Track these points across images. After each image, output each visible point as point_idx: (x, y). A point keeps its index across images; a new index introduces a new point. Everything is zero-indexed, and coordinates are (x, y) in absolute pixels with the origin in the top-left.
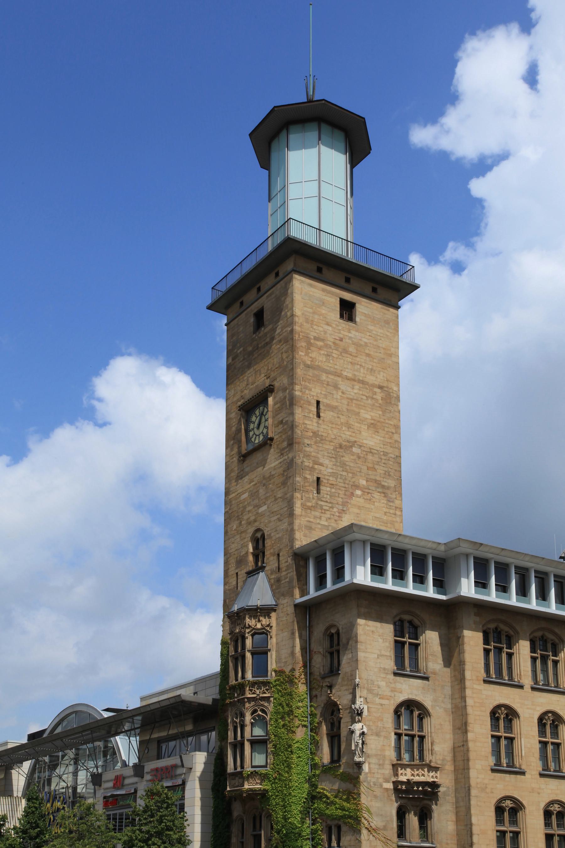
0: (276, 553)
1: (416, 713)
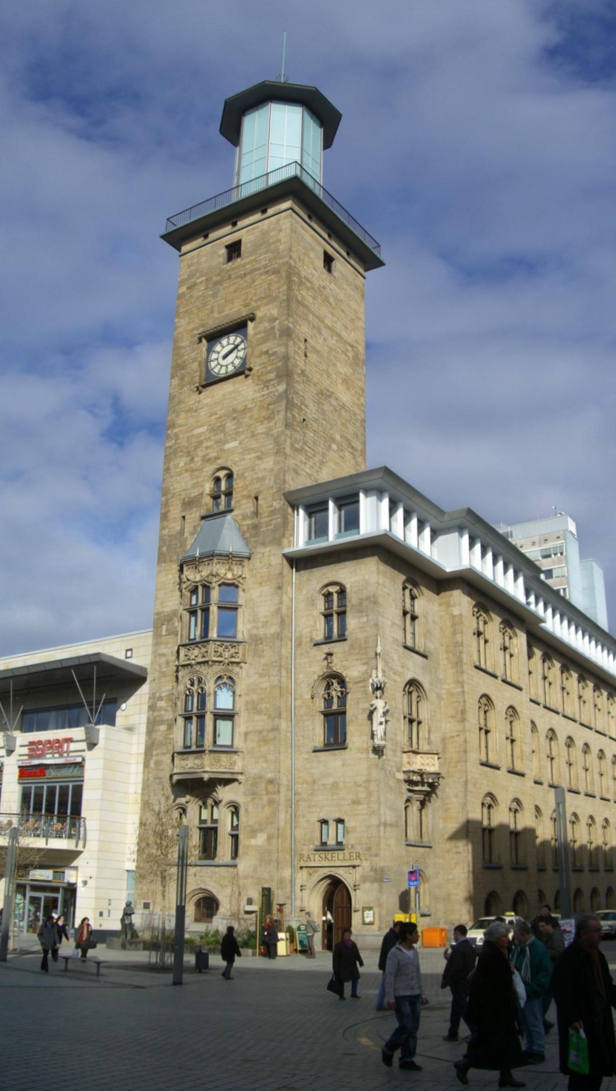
0: (253, 495)
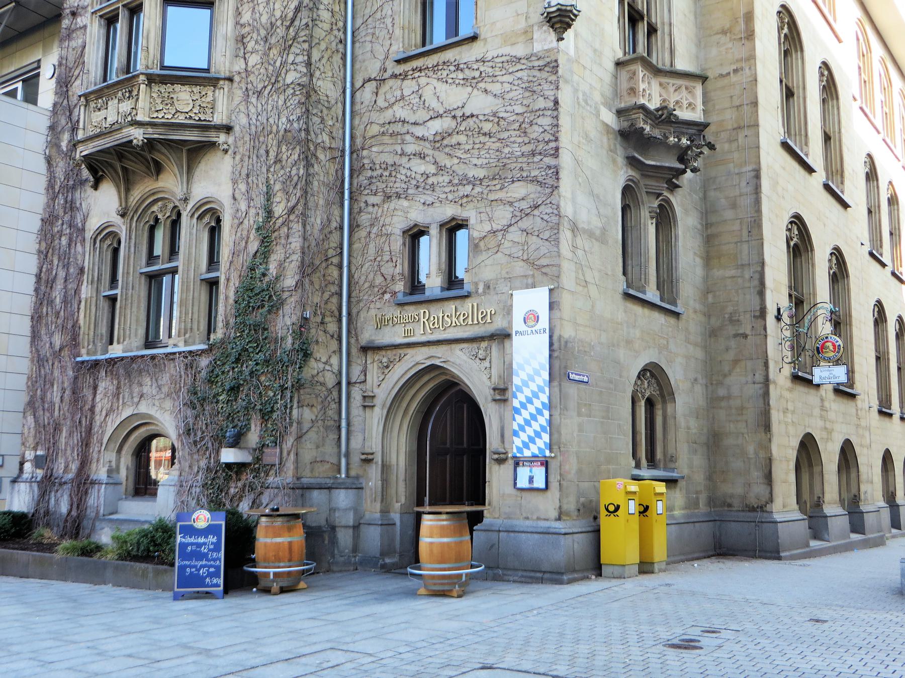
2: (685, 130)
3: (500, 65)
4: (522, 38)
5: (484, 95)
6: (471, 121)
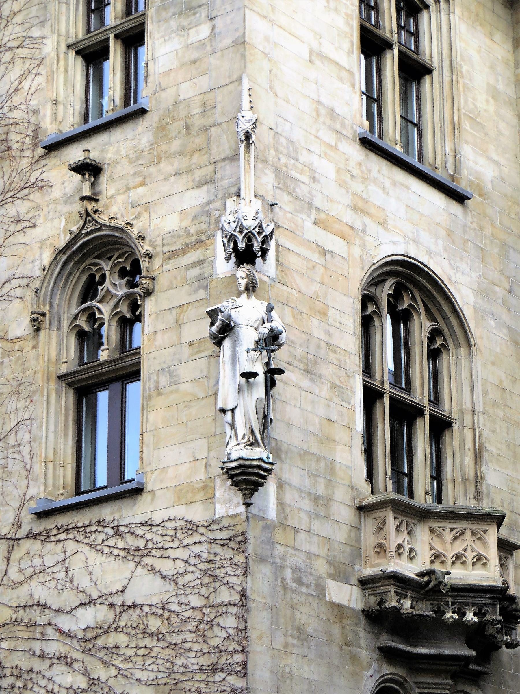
1: (421, 327)
2: (471, 601)
3: (172, 533)
4: (200, 496)
5: (151, 576)
6: (134, 614)
